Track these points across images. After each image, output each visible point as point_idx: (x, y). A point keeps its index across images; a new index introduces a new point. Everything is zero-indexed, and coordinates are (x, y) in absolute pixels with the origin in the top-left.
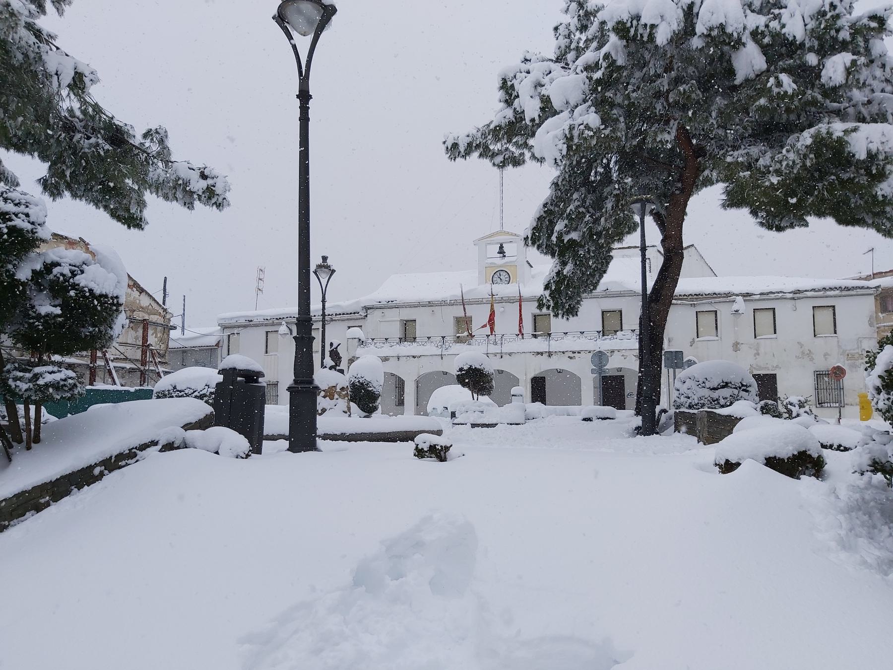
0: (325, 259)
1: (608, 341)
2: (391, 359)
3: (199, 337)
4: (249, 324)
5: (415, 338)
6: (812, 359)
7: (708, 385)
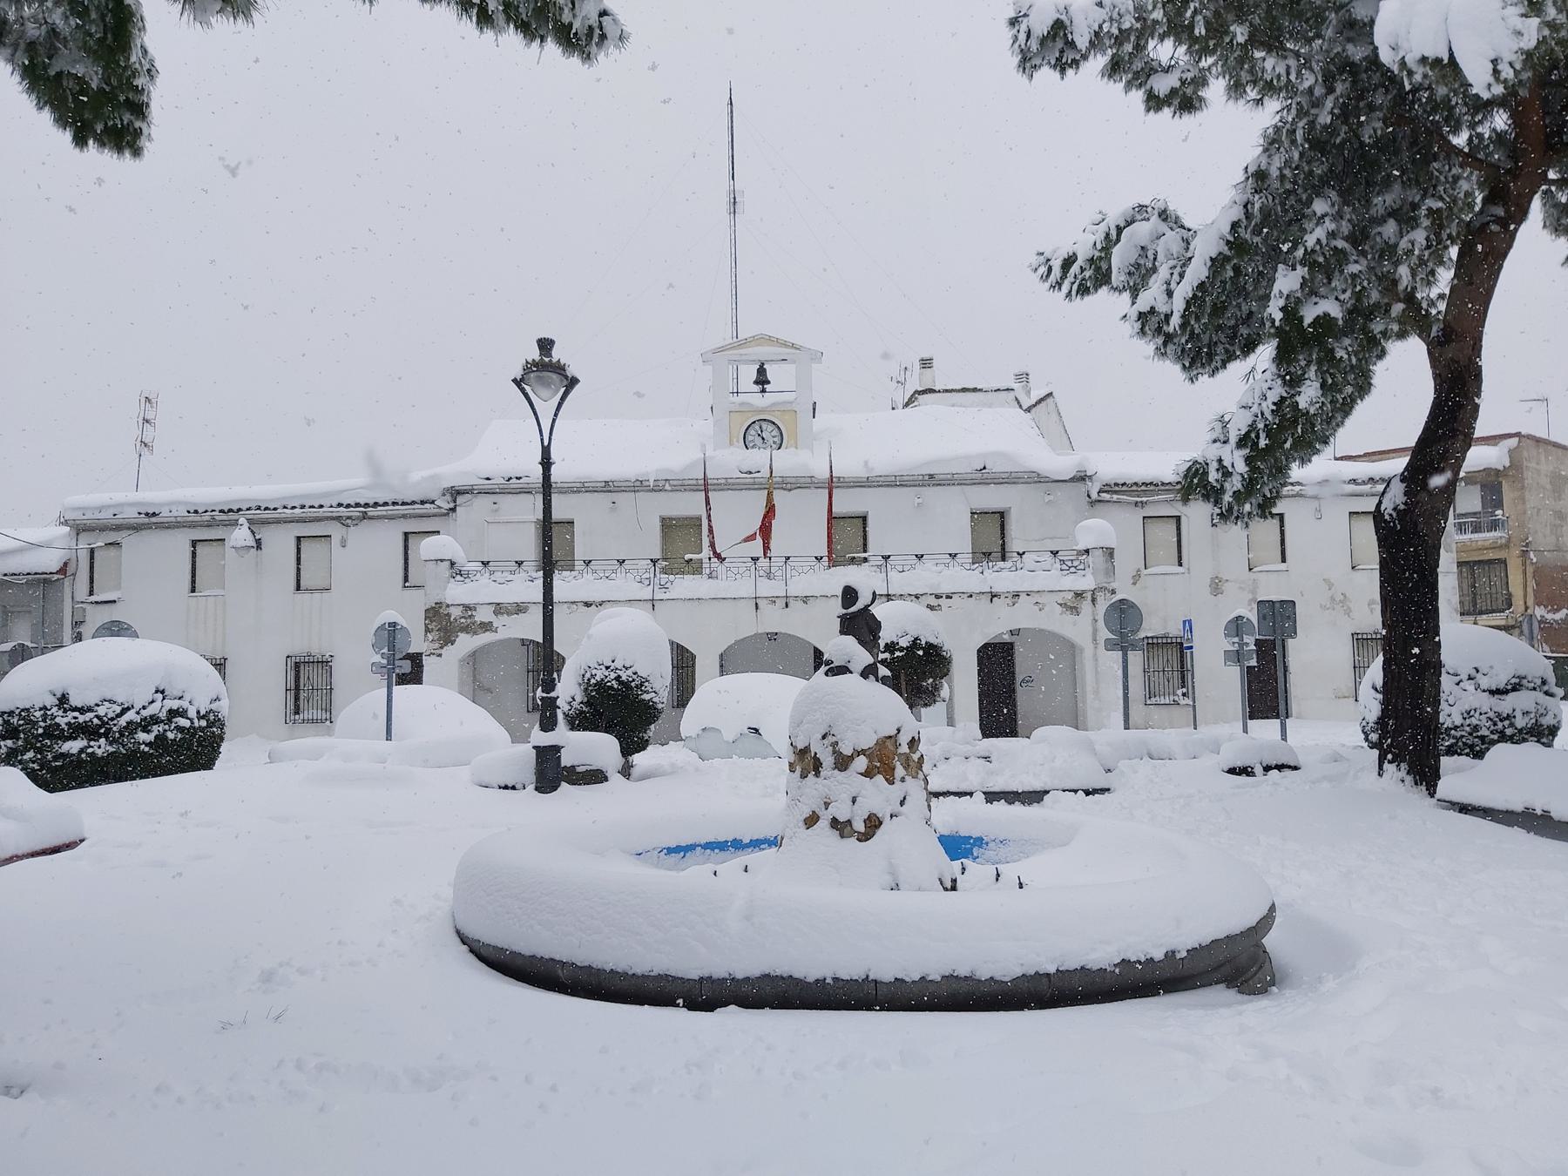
0: (545, 345)
1: (1005, 574)
3: (20, 550)
4: (150, 521)
6: (1348, 612)
7: (1485, 683)
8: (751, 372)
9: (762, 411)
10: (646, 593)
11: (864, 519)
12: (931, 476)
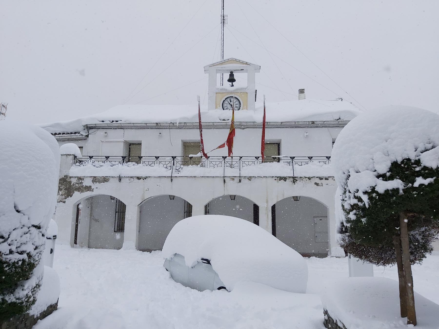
2: (111, 179)
5: (140, 158)
8: (227, 76)
9: (231, 93)
10: (169, 173)
11: (279, 145)
12: (313, 122)
